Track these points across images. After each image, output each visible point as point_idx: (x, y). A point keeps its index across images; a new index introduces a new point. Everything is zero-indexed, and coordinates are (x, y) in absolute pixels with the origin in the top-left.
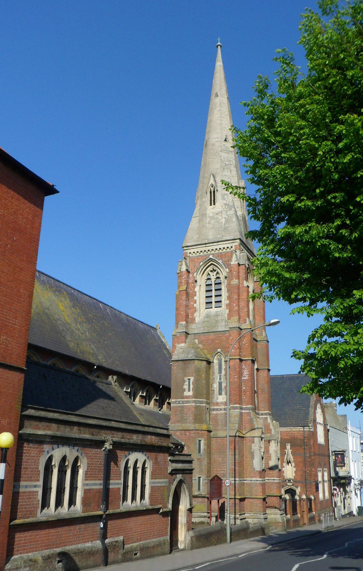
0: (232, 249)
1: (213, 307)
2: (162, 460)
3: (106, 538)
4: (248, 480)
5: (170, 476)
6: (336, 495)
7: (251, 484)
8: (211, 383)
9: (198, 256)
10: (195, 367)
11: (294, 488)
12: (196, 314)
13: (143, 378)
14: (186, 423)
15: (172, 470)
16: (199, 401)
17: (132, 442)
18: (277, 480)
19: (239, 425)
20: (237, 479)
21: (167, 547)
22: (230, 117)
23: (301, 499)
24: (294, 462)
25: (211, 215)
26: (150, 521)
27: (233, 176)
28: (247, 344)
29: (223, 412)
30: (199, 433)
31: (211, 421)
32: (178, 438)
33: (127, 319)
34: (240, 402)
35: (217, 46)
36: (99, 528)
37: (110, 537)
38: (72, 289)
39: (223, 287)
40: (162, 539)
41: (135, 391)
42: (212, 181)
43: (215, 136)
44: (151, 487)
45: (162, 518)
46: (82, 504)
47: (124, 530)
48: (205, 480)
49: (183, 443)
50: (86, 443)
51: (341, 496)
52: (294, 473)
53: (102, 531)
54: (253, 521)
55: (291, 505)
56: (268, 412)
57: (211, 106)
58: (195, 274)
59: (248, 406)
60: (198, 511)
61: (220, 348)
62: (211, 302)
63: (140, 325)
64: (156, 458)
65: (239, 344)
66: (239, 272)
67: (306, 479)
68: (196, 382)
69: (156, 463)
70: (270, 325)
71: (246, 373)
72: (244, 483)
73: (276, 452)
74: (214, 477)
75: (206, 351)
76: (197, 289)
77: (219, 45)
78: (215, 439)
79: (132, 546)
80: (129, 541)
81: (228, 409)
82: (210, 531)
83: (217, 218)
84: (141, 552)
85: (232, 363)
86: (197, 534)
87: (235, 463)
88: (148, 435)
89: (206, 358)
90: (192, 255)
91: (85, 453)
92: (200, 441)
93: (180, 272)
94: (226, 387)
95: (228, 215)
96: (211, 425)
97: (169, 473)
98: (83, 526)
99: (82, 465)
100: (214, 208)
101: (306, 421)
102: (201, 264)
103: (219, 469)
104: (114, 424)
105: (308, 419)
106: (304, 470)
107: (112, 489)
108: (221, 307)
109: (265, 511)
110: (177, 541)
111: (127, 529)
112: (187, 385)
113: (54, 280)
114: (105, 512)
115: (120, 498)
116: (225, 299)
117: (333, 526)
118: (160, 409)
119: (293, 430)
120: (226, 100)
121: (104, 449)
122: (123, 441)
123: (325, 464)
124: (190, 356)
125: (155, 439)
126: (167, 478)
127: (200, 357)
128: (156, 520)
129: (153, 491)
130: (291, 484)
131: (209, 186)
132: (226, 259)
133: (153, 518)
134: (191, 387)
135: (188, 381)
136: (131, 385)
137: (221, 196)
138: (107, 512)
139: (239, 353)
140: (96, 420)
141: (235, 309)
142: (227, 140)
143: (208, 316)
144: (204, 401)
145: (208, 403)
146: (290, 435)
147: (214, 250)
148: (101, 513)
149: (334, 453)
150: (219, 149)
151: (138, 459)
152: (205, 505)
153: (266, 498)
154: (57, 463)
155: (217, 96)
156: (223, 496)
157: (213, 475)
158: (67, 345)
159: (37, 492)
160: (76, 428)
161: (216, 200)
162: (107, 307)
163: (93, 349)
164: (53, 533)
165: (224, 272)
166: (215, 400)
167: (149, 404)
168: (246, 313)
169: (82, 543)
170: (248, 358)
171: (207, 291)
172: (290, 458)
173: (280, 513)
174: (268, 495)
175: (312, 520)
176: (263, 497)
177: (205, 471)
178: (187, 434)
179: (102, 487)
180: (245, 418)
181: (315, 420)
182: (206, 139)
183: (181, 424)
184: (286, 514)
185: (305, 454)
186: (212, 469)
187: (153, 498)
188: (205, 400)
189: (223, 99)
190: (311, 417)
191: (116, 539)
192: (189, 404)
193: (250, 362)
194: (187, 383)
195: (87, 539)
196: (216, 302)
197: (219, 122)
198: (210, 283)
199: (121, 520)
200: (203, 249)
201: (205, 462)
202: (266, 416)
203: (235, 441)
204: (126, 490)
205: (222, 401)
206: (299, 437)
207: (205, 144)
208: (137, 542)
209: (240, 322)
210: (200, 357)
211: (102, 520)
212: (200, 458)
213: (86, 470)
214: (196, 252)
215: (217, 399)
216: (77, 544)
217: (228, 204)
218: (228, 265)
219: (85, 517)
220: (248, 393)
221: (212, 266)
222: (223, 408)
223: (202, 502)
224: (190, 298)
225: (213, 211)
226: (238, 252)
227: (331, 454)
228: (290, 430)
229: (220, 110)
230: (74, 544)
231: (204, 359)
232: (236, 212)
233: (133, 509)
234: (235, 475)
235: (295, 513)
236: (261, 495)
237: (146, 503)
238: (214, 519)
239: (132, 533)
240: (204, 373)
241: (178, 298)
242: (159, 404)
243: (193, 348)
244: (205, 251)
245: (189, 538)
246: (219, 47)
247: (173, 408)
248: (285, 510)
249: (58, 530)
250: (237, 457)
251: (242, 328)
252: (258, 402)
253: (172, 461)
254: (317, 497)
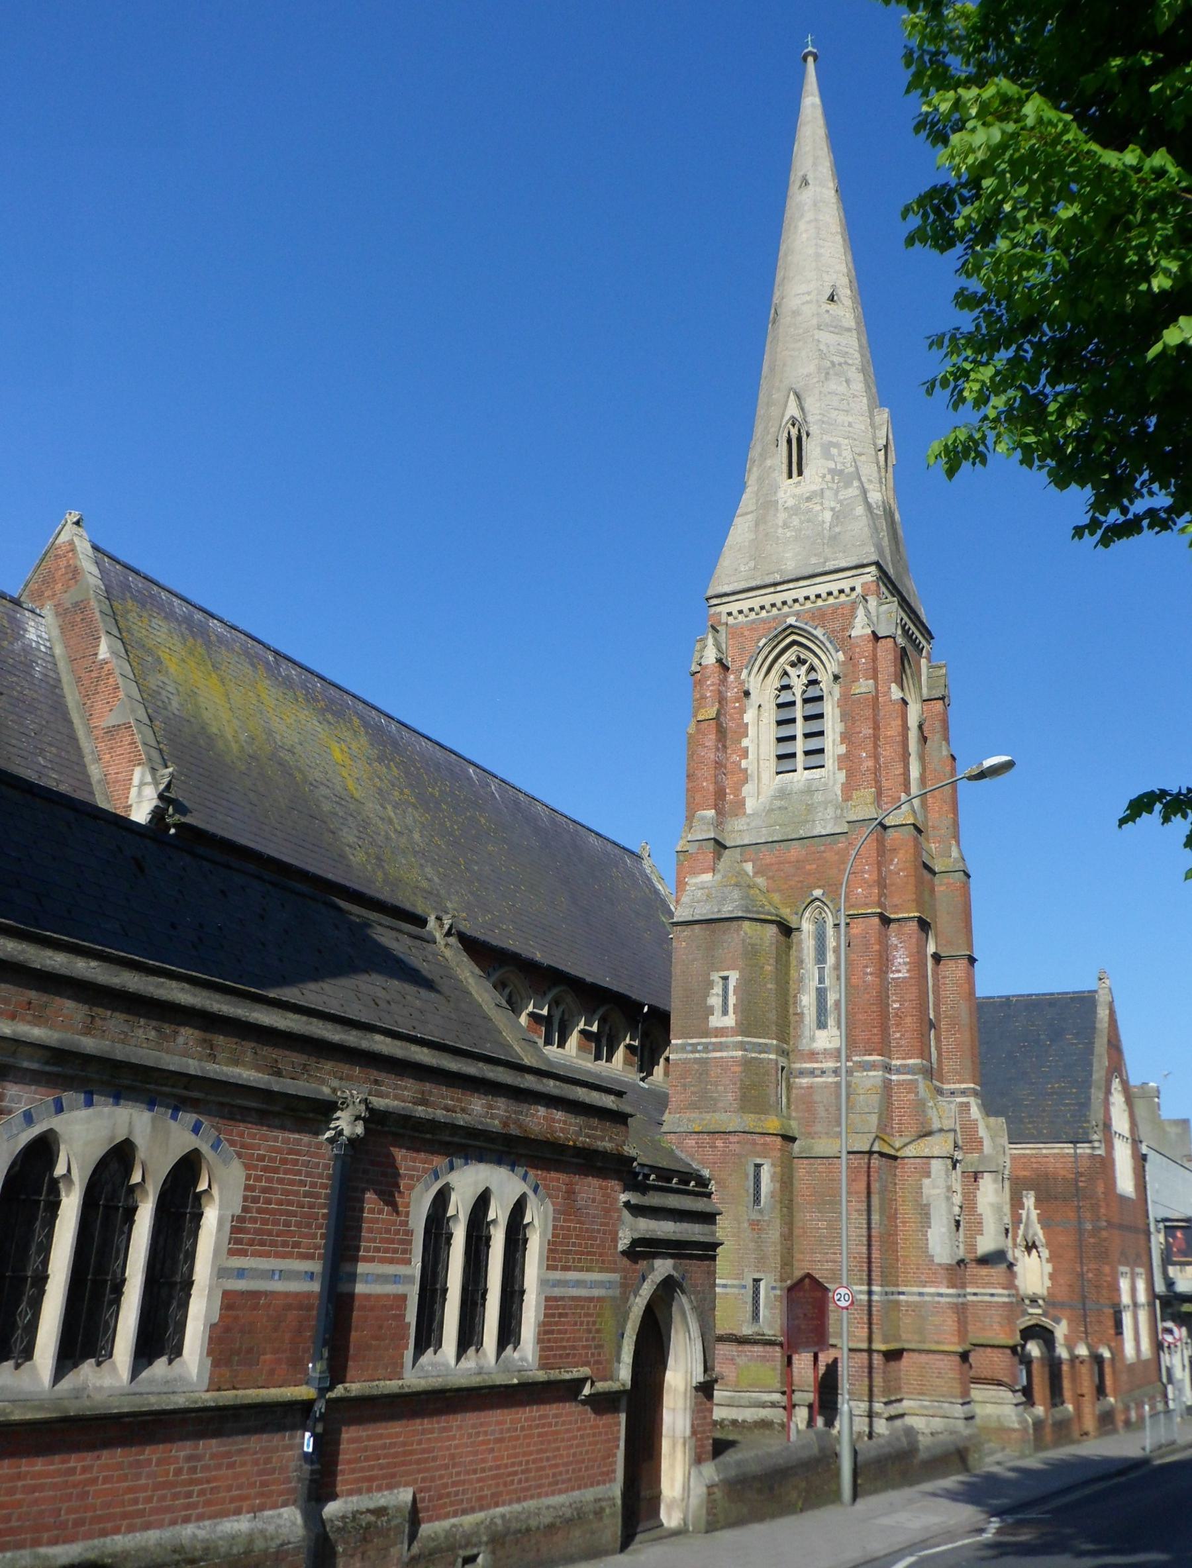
0: (854, 595)
1: (800, 766)
2: (594, 1201)
3: (333, 1497)
4: (910, 1294)
5: (626, 1262)
6: (1172, 1346)
7: (917, 1305)
8: (792, 993)
9: (753, 621)
10: (743, 941)
11: (1047, 1322)
12: (748, 790)
13: (589, 979)
14: (714, 1112)
15: (635, 1243)
16: (754, 1044)
17: (461, 1119)
18: (1001, 1296)
19: (880, 1119)
20: (875, 1288)
21: (613, 1526)
22: (844, 240)
23: (1074, 1358)
24: (1048, 1245)
25: (791, 502)
26: (537, 1426)
27: (854, 396)
28: (901, 870)
29: (830, 1080)
30: (754, 1143)
31: (793, 1107)
32: (692, 1156)
33: (553, 821)
34: (884, 1048)
35: (805, 59)
36: (296, 1453)
37: (350, 1493)
38: (382, 716)
39: (830, 708)
40: (589, 1495)
41: (566, 1017)
42: (792, 410)
43: (803, 288)
44: (547, 1299)
45: (593, 1416)
46: (210, 1353)
47: (418, 1462)
48: (774, 1288)
49: (706, 1173)
50: (239, 1102)
51: (1182, 1350)
52: (1046, 1278)
53: (307, 1467)
54: (927, 1425)
55: (1047, 1376)
56: (972, 1086)
57: (788, 214)
58: (745, 672)
59: (911, 1061)
60: (751, 1386)
61: (819, 887)
62: (793, 755)
63: (592, 839)
64: (570, 1193)
65: (879, 871)
66: (874, 659)
67: (1084, 1298)
68: (746, 986)
69: (568, 1209)
70: (982, 775)
71: (902, 961)
72: (898, 1303)
73: (998, 1209)
74: (802, 1280)
75: (776, 897)
76: (749, 717)
77: (810, 53)
78: (805, 1161)
79: (454, 1526)
80: (444, 1506)
81: (844, 1070)
82: (781, 1461)
83: (810, 510)
84: (493, 1552)
85: (858, 928)
86: (733, 1473)
87: (869, 1237)
88: (538, 1103)
89: (777, 916)
90: (735, 618)
91: (232, 1143)
92: (758, 1166)
93: (698, 668)
94: (837, 1003)
95: (840, 502)
96: (795, 1119)
97: (623, 1253)
98: (210, 1447)
99: (215, 1191)
100: (799, 482)
101: (1083, 1128)
102: (761, 644)
103: (818, 1257)
104: (381, 1044)
105: (1088, 1122)
106: (1079, 1270)
107: (368, 1297)
108: (823, 766)
109: (965, 1393)
110: (655, 1501)
111: (434, 1459)
112: (718, 995)
113: (323, 682)
114: (322, 1391)
115: (405, 1337)
116: (834, 740)
117: (1173, 1443)
118: (642, 1075)
119: (1044, 1151)
120: (833, 192)
121: (328, 1135)
122: (420, 1111)
123: (1138, 1256)
124: (727, 910)
125: (565, 1122)
126: (614, 1271)
127: (758, 913)
128: (564, 1423)
129: (553, 1315)
130: (1039, 1311)
131: (784, 424)
132: (837, 626)
133: (556, 1416)
134: (732, 1000)
135: (721, 982)
136: (550, 996)
137: (818, 449)
138: (339, 1391)
139: (880, 899)
140: (296, 1017)
141: (864, 767)
142: (835, 298)
143: (783, 794)
144: (771, 1044)
145: (784, 1053)
146: (1035, 1166)
147: (802, 600)
148: (305, 1392)
149: (1161, 1225)
150: (815, 322)
151: (493, 1188)
152: (774, 1369)
153: (969, 1351)
154: (81, 1169)
155: (807, 184)
156: (832, 1341)
157: (798, 1274)
158: (343, 856)
160: (187, 1035)
161: (804, 461)
162: (490, 779)
163: (429, 880)
164: (40, 1475)
165: (830, 663)
166: (804, 1045)
167: (609, 1060)
168: (901, 779)
169: (200, 1518)
170: (906, 915)
171: (780, 723)
172: (1035, 1234)
173: (1015, 1401)
174: (975, 1342)
175: (1106, 1420)
176: (960, 1350)
177: (775, 1261)
178: (719, 1143)
179: (315, 1287)
180: (902, 1099)
181: (1107, 1126)
182: (775, 300)
183: (701, 1113)
184: (1033, 1404)
185: (1080, 1223)
186: (797, 1256)
187: (556, 1340)
188: (775, 1042)
189: (824, 190)
190: (1096, 1115)
191: (382, 1499)
192: (724, 1054)
193: (914, 925)
194: (718, 989)
195: (232, 1500)
196: (807, 753)
197: (811, 251)
198: (791, 699)
199: (404, 1422)
200: (767, 601)
201: (774, 1234)
202: (964, 1100)
203: (869, 1168)
204: (437, 1306)
205: (828, 1046)
206: (1062, 1172)
207: (772, 316)
208: (482, 1509)
209: (879, 806)
210: (758, 913)
211: (310, 1423)
212: (759, 1221)
213: (238, 1211)
214: (746, 610)
215: (813, 1039)
216: (173, 1523)
217: (841, 471)
218: (843, 641)
219: (218, 1408)
220: (909, 1020)
221: (795, 647)
222: (829, 1068)
223: (764, 1359)
224: (728, 743)
225: (798, 491)
226: (872, 602)
227: (1152, 1229)
228: (1034, 1152)
229: (816, 220)
230: (160, 1525)
231: (769, 917)
232: (864, 492)
233: (464, 1382)
234: (869, 1275)
235: (1058, 1400)
236: (954, 1344)
237: (522, 1359)
238: (802, 1414)
239: (458, 1474)
240: (772, 961)
241: (693, 742)
242: (641, 1060)
243: (737, 885)
244: (773, 605)
245: (699, 1491)
246: (810, 59)
247: (676, 1064)
248: (1027, 1391)
249: (72, 1464)
250: (875, 1217)
251: (887, 822)
252: (939, 1055)
253: (637, 1210)
254: (1117, 1352)
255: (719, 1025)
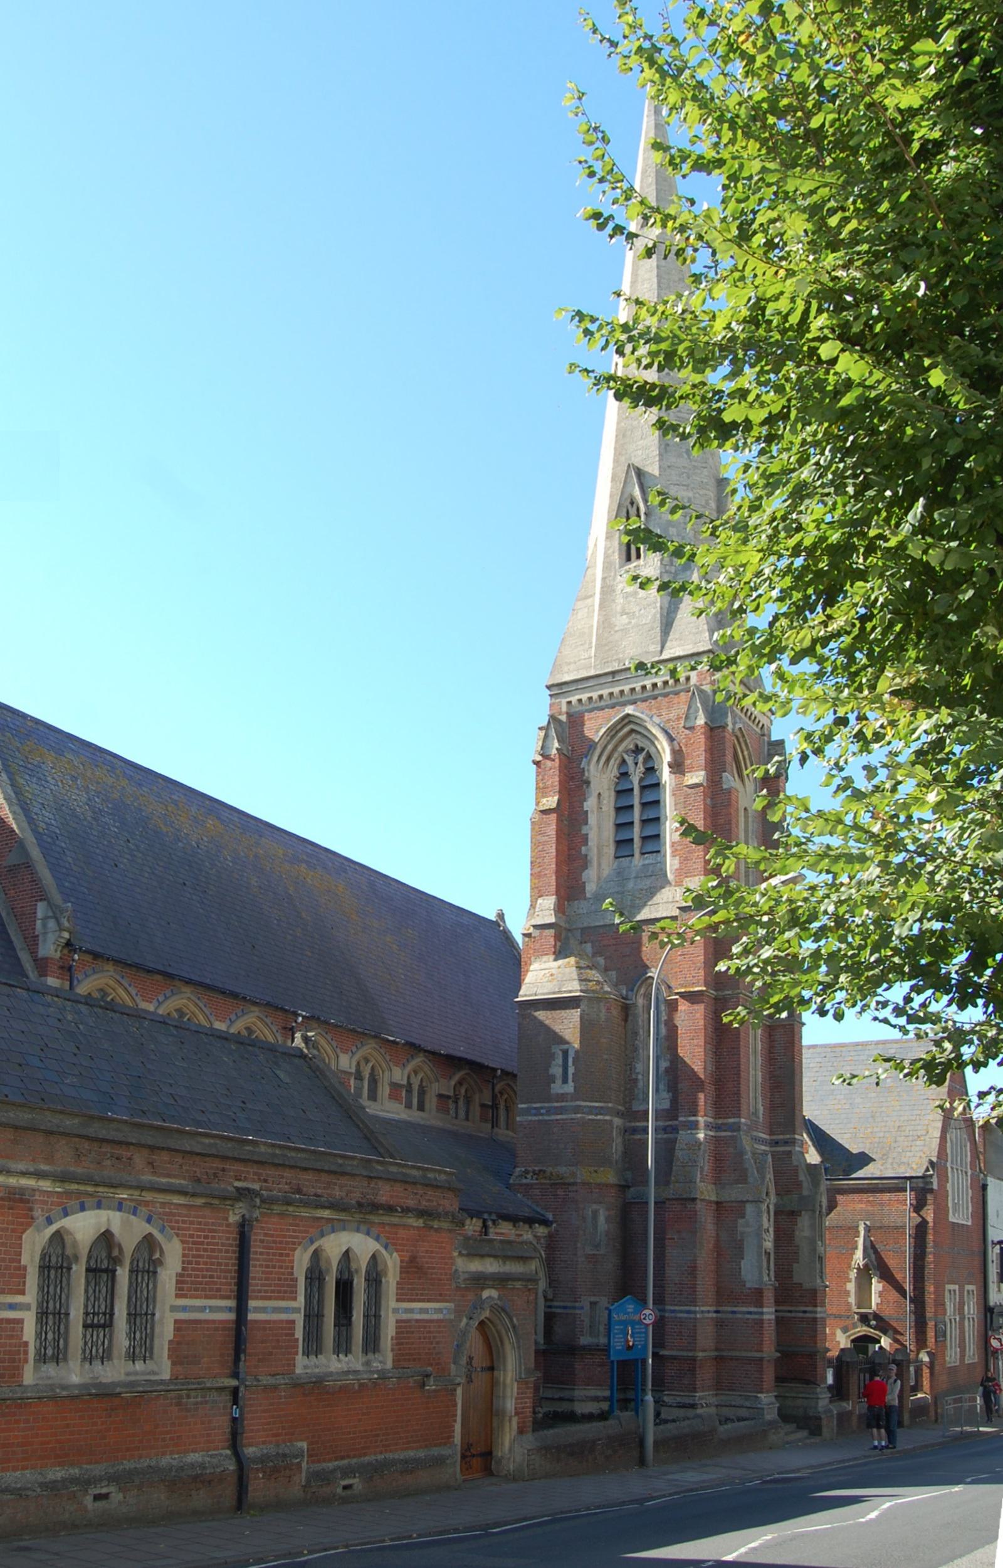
91: (172, 1228)
107: (256, 1321)
159: (20, 1321)
178: (560, 1192)
213: (179, 1270)
221: (633, 735)
255: (561, 1091)
